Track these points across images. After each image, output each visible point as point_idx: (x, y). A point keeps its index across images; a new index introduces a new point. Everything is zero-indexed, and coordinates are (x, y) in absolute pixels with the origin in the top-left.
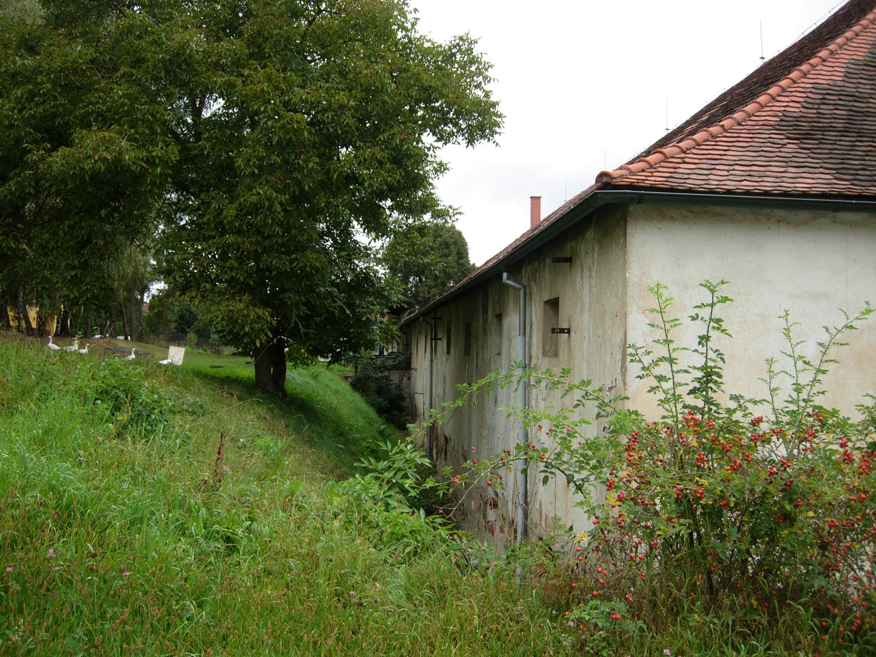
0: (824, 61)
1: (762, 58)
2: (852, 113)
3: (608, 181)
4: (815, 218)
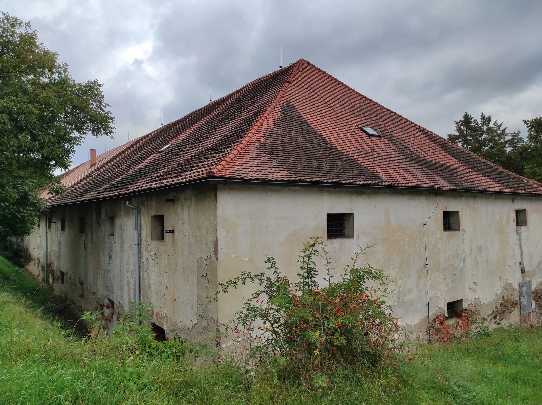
0: (267, 118)
1: (210, 100)
2: (282, 142)
3: (213, 175)
4: (283, 189)
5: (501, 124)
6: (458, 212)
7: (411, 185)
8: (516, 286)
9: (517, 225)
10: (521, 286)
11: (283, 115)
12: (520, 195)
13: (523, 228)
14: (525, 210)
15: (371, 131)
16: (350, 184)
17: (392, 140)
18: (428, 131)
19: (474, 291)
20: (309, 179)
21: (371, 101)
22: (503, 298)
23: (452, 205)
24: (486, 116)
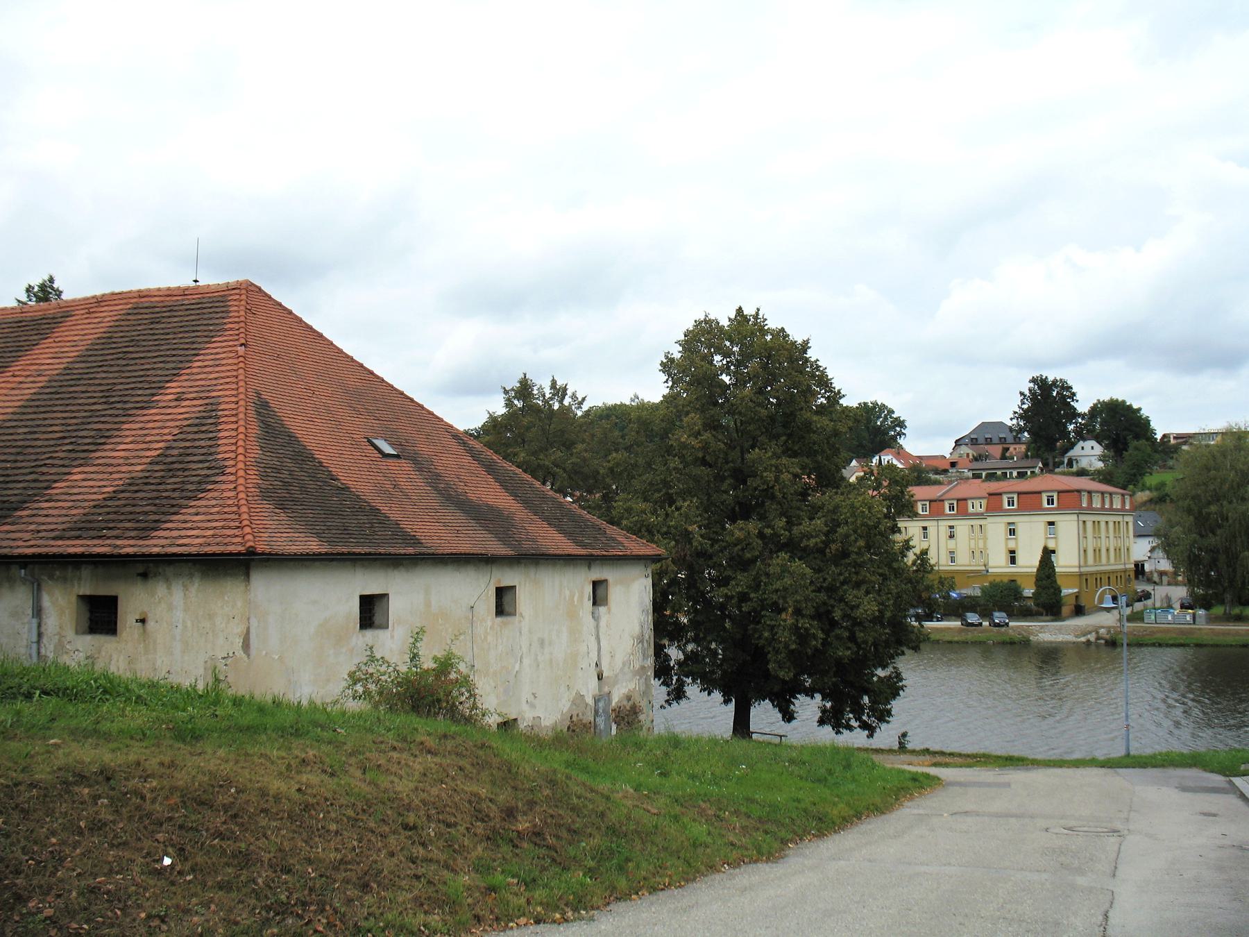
5: (584, 399)
6: (514, 587)
8: (590, 701)
9: (594, 603)
10: (597, 700)
11: (261, 425)
12: (598, 559)
13: (602, 609)
14: (606, 580)
15: (388, 450)
16: (390, 554)
17: (415, 459)
19: (533, 706)
20: (345, 550)
21: (372, 373)
22: (571, 718)
23: (508, 577)
24: (560, 383)
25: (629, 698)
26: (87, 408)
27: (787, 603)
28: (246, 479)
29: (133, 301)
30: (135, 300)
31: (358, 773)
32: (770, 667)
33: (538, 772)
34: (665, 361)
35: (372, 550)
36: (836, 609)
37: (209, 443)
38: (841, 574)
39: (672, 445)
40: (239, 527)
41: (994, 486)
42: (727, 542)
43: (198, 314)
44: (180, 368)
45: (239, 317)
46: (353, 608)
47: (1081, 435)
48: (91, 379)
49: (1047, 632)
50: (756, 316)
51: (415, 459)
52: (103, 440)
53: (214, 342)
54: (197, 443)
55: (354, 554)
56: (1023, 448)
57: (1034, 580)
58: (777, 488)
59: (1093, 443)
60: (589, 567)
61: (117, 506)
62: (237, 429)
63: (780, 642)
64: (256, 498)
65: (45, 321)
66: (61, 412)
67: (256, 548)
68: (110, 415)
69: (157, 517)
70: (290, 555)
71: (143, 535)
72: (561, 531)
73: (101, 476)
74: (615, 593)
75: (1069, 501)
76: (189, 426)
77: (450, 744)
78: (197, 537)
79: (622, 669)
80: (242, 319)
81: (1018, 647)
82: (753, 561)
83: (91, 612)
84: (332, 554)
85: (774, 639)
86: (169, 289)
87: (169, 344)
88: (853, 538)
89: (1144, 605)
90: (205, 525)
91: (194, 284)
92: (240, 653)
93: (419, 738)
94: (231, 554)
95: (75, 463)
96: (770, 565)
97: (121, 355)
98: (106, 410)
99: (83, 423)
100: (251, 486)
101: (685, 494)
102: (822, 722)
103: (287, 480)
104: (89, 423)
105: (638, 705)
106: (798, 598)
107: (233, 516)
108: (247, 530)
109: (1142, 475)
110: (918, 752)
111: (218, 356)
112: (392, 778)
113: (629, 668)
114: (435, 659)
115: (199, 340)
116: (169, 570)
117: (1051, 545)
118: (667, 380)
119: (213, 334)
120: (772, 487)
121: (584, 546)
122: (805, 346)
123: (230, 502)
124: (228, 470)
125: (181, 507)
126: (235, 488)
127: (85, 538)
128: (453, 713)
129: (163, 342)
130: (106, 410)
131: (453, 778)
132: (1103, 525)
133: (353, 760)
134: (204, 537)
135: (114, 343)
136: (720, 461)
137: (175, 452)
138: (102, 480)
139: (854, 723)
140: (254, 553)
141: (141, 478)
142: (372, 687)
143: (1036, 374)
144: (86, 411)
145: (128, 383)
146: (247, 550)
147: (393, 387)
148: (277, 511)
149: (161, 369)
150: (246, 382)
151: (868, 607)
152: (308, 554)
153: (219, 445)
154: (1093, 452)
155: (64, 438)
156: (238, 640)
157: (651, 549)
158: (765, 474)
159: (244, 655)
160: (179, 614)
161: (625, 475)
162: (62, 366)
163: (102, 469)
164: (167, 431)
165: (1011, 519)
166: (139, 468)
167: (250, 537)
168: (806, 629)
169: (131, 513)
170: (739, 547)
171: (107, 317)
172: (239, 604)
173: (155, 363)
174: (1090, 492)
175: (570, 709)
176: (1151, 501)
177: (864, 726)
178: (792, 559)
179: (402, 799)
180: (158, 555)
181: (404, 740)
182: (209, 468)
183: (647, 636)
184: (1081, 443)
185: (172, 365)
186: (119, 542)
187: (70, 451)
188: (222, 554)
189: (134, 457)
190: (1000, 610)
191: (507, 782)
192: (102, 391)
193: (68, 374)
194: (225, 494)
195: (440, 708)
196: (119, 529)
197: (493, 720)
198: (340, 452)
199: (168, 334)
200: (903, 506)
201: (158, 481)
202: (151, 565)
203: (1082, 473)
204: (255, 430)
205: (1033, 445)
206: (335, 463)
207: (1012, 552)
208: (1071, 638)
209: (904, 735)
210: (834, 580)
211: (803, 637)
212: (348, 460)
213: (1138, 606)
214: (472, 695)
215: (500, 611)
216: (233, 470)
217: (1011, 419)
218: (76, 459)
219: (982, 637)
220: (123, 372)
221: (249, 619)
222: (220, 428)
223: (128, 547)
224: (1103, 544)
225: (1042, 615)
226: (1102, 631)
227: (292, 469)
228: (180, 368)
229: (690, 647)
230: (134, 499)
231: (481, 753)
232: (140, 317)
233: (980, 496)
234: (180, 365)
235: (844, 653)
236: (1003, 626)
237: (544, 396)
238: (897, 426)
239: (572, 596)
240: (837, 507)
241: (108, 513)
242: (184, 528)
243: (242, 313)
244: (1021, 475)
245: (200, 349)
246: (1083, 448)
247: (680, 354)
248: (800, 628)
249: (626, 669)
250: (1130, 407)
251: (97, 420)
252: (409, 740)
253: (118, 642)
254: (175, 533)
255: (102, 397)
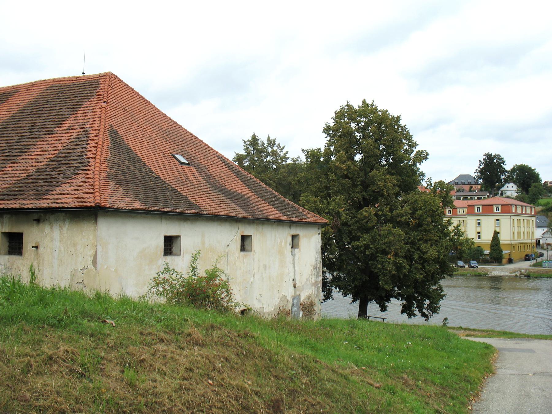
5: (283, 147)
6: (251, 236)
7: (221, 214)
8: (290, 299)
9: (292, 247)
11: (112, 142)
14: (298, 235)
15: (183, 160)
16: (182, 213)
17: (198, 167)
18: (225, 158)
19: (260, 301)
20: (156, 209)
21: (176, 123)
22: (280, 308)
23: (248, 230)
25: (309, 298)
26: (20, 135)
27: (391, 249)
28: (100, 168)
29: (50, 84)
30: (52, 83)
31: (115, 372)
32: (380, 283)
33: (294, 359)
34: (325, 127)
35: (172, 210)
36: (415, 254)
37: (82, 150)
38: (418, 235)
39: (331, 167)
40: (92, 193)
41: (470, 202)
42: (359, 218)
43: (83, 88)
44: (71, 114)
45: (104, 89)
46: (161, 242)
47: (507, 181)
48: (24, 121)
49: (495, 270)
50: (372, 105)
51: (198, 167)
52: (25, 150)
53: (90, 101)
54: (75, 151)
55: (161, 211)
56: (479, 187)
57: (490, 246)
58: (385, 190)
59: (513, 184)
60: (290, 227)
61: (27, 183)
62: (98, 143)
63: (387, 270)
64: (105, 178)
65: (5, 95)
66: (6, 137)
67: (101, 204)
68: (31, 138)
69: (48, 188)
70: (122, 209)
71: (39, 198)
72: (276, 208)
73: (21, 168)
74: (303, 242)
75: (506, 209)
76: (72, 142)
77: (216, 334)
78: (69, 198)
79: (306, 283)
80: (106, 90)
81: (480, 276)
82: (373, 227)
83: (9, 242)
84: (147, 210)
85: (383, 269)
86: (69, 78)
87: (66, 103)
88: (425, 216)
89: (542, 259)
90: (74, 192)
91: (82, 75)
92: (91, 267)
93: (188, 329)
94: (86, 207)
95: (8, 162)
96: (381, 230)
97: (40, 109)
98: (29, 135)
99: (17, 142)
100: (102, 172)
101: (336, 193)
102: (403, 312)
103: (124, 171)
104: (20, 142)
105: (313, 301)
106: (397, 247)
107: (90, 187)
108: (97, 194)
109: (538, 199)
110: (456, 328)
111: (91, 108)
112: (154, 375)
113: (310, 282)
114: (207, 272)
115: (82, 100)
116: (52, 217)
117: (498, 230)
118: (327, 136)
119: (90, 97)
120: (382, 190)
121: (288, 216)
122: (398, 119)
123: (90, 180)
124: (91, 164)
125: (62, 183)
126: (93, 172)
127: (6, 200)
128: (217, 304)
129: (63, 102)
130: (29, 135)
131: (220, 372)
132: (522, 221)
133: (113, 355)
134: (72, 198)
135: (38, 103)
136: (356, 176)
137: (63, 155)
138: (22, 170)
139: (416, 312)
140: (100, 207)
141: (43, 169)
142: (168, 288)
143: (487, 152)
144: (19, 136)
145: (43, 122)
146: (95, 205)
147: (187, 131)
148: (117, 186)
149: (61, 115)
150: (105, 120)
151: (432, 253)
152: (133, 209)
153: (87, 151)
154: (512, 189)
155: (6, 150)
156: (90, 259)
157: (321, 220)
158: (379, 183)
159: (93, 268)
160: (57, 243)
161: (306, 184)
162: (10, 115)
163: (23, 164)
164: (60, 145)
165: (478, 218)
166: (43, 164)
167: (98, 198)
168: (401, 264)
169: (34, 186)
170: (365, 221)
171: (36, 92)
172: (91, 237)
173: (58, 112)
174: (516, 206)
175: (279, 303)
176: (542, 211)
177: (423, 315)
178: (394, 227)
179: (162, 404)
180: (45, 208)
181: (173, 331)
182: (80, 163)
183: (318, 266)
184: (507, 185)
185: (67, 113)
186: (24, 202)
187: (8, 156)
188: (81, 207)
189: (41, 158)
190: (473, 260)
191: (270, 371)
192: (29, 126)
193: (12, 119)
194: (87, 176)
195: (209, 302)
196: (26, 194)
197: (238, 309)
198: (156, 159)
199: (67, 98)
200: (448, 202)
201: (52, 170)
202: (42, 215)
203: (508, 197)
204: (108, 144)
205: (484, 185)
206: (153, 164)
207: (479, 233)
208: (508, 274)
209: (446, 319)
210: (414, 238)
211: (399, 268)
212: (160, 164)
213: (539, 260)
214: (229, 294)
215: (243, 248)
216: (93, 164)
217: (475, 173)
218: (10, 160)
219: (465, 272)
220: (41, 117)
221: (96, 246)
222: (89, 142)
223: (29, 204)
224: (522, 230)
225: (493, 263)
226: (523, 271)
227: (128, 165)
228: (71, 114)
229: (335, 273)
230: (37, 179)
231: (243, 342)
232: (53, 91)
233: (463, 206)
234: (71, 113)
235: (419, 277)
236: (475, 267)
237: (263, 145)
238: (421, 175)
239: (281, 242)
240: (416, 201)
241: (22, 187)
242: (62, 194)
243: (106, 87)
244: (479, 198)
245: (82, 105)
246: (508, 187)
247: (334, 124)
248: (397, 263)
249: (308, 283)
250: (530, 168)
251: (24, 140)
252: (177, 331)
253: (23, 260)
254: (56, 197)
255: (28, 129)
